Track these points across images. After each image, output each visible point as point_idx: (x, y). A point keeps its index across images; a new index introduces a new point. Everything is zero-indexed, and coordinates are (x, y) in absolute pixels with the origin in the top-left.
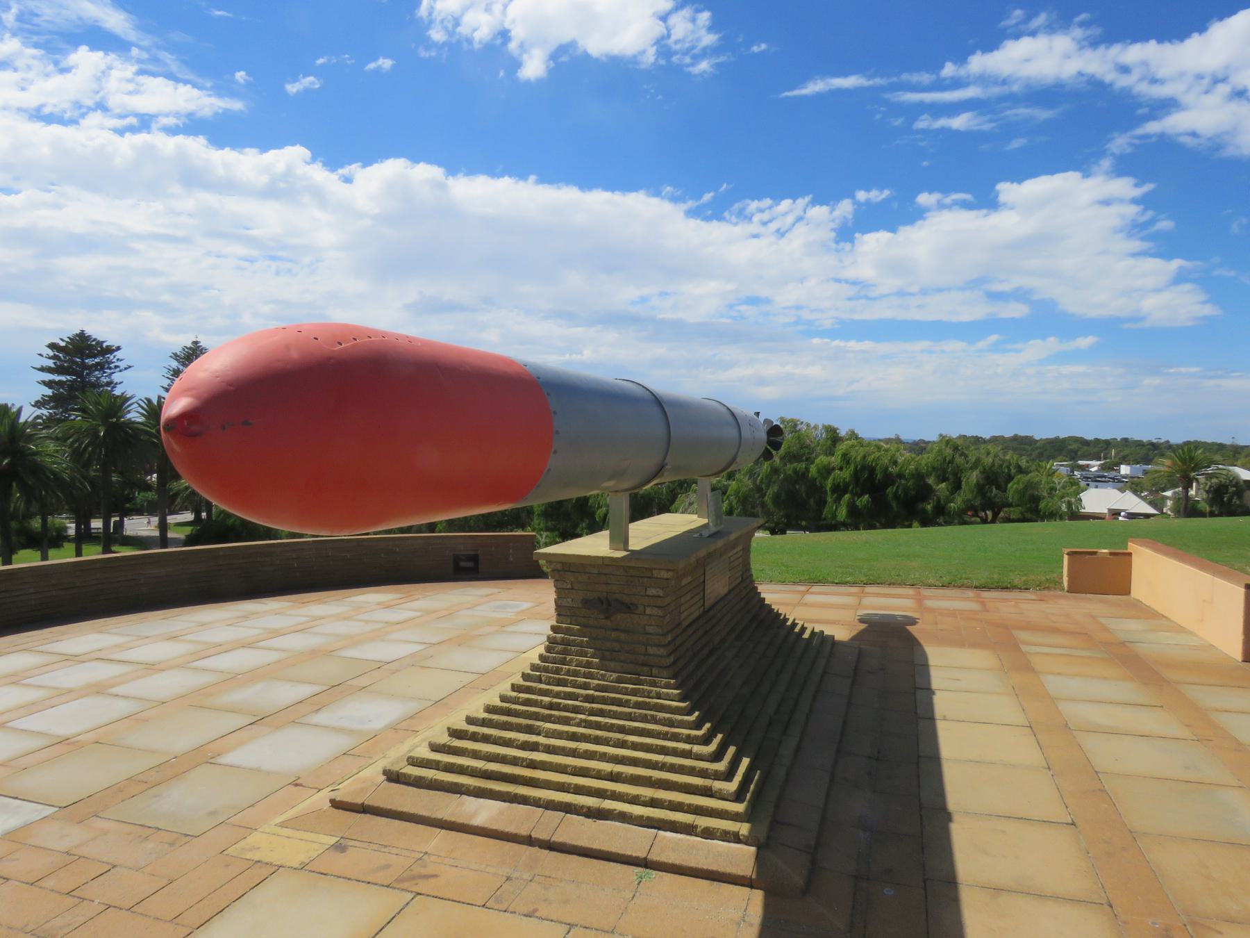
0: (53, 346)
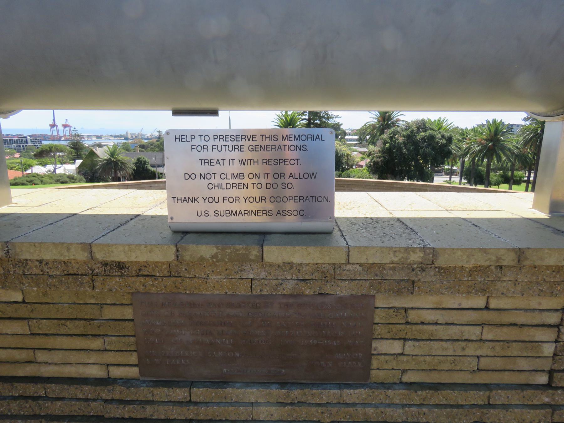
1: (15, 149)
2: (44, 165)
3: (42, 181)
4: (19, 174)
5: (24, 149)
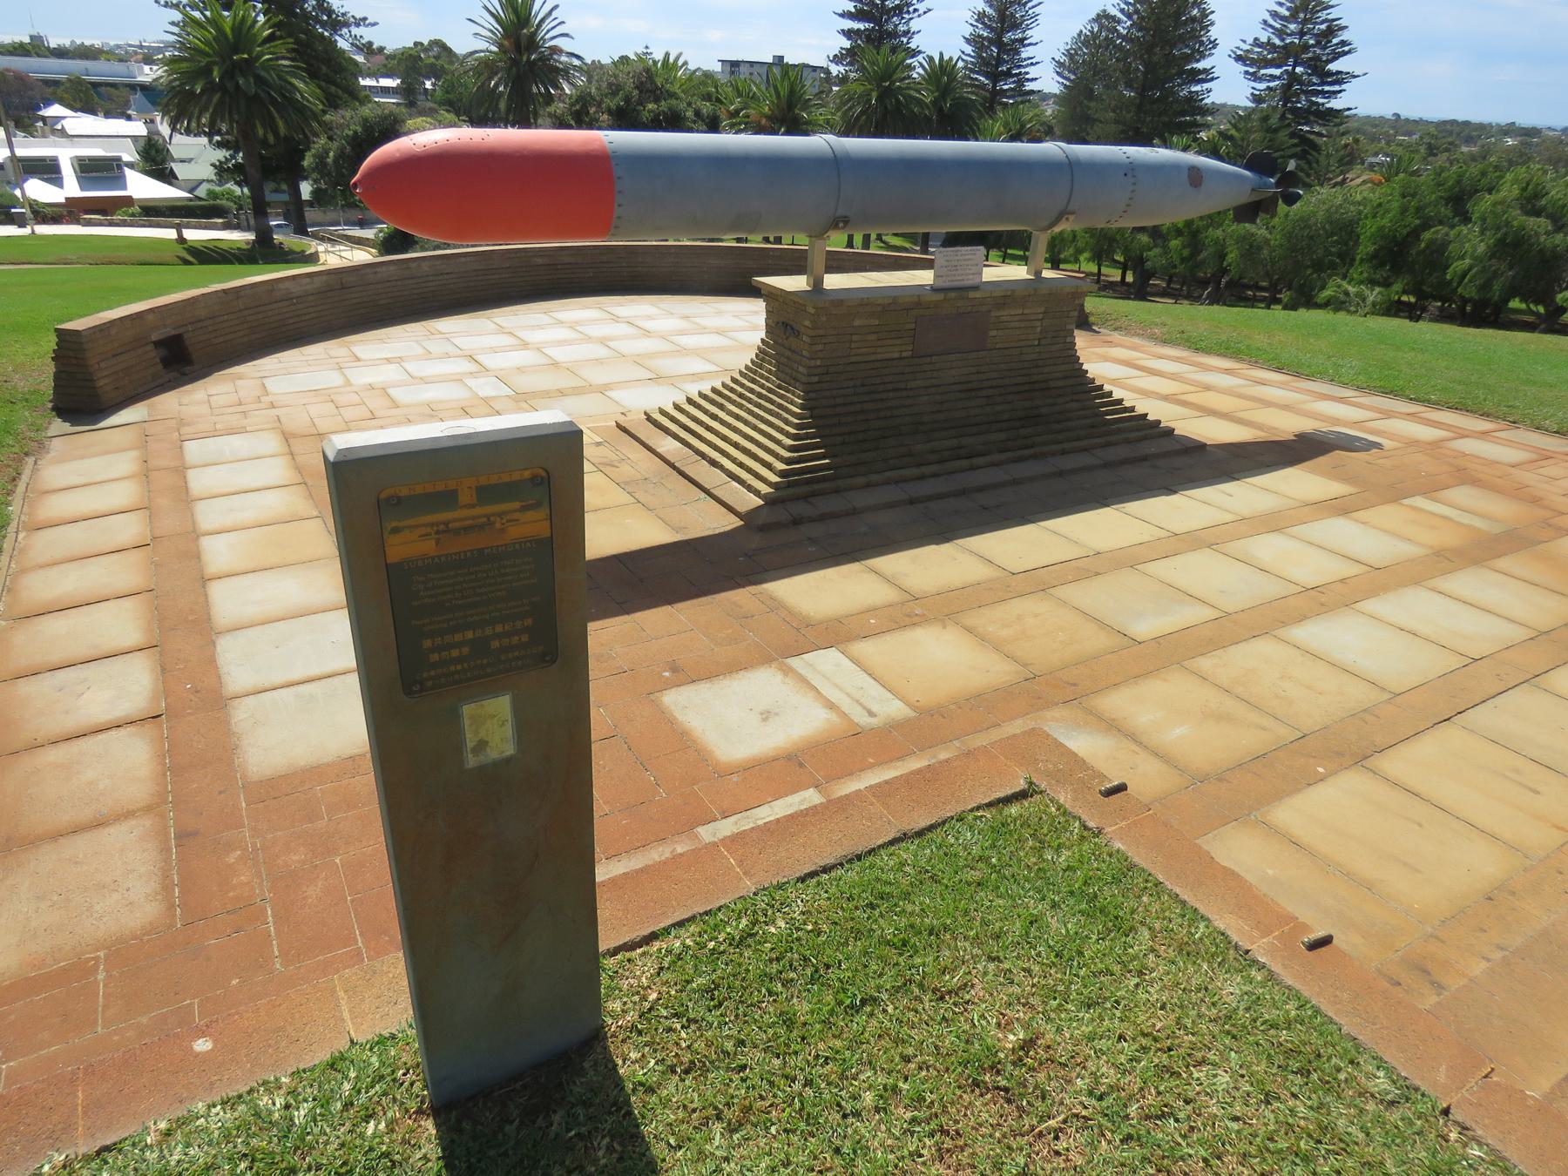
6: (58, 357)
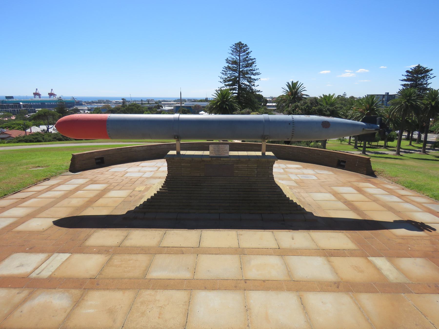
0: (407, 72)
1: (11, 112)
2: (38, 125)
3: (43, 139)
4: (22, 133)
5: (18, 112)
6: (72, 160)
